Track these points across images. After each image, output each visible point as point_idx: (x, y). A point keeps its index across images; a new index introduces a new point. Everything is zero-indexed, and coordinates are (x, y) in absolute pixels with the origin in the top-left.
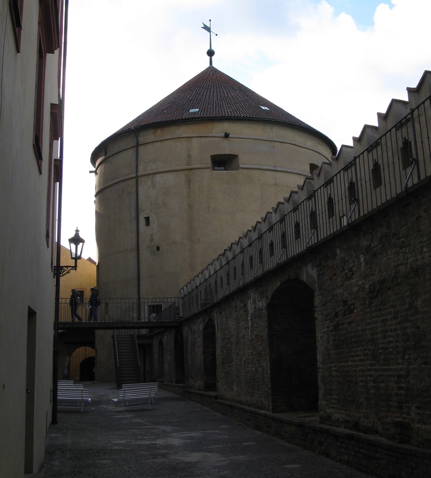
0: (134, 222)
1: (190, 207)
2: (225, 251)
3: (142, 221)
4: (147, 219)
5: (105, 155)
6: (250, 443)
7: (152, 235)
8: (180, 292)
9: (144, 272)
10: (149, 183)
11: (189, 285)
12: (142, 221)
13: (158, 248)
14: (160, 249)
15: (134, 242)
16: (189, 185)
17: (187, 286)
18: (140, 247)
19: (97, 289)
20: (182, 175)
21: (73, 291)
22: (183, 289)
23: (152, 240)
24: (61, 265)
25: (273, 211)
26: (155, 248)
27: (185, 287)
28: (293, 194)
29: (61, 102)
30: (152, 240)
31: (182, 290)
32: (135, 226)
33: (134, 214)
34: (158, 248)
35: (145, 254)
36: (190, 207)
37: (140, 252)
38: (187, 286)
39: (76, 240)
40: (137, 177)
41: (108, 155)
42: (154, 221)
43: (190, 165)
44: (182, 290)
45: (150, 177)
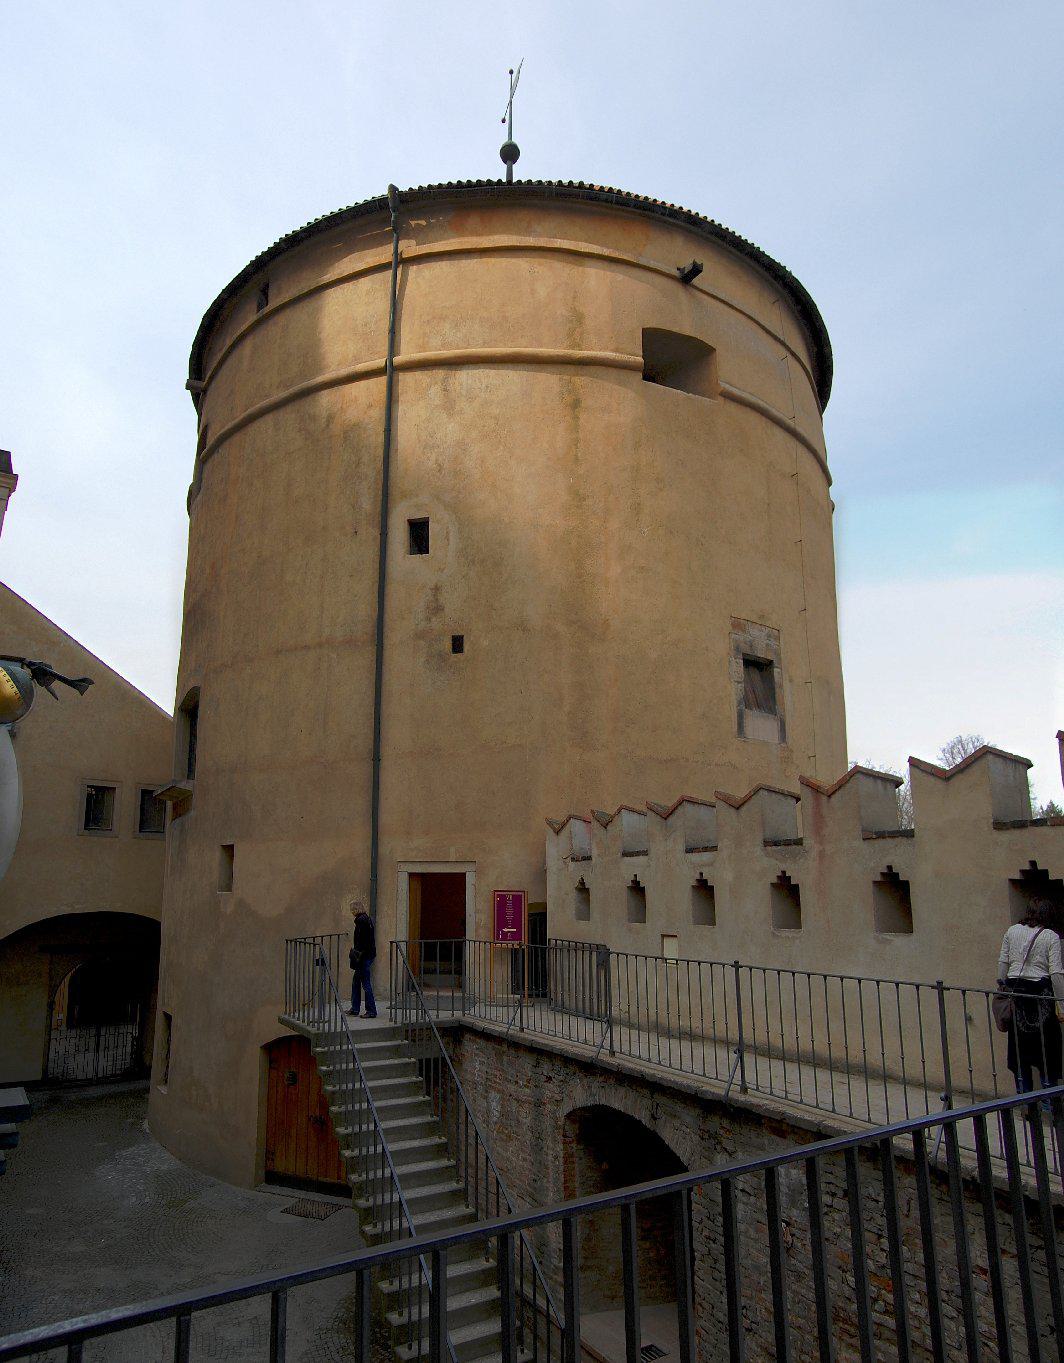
0: (371, 533)
3: (399, 535)
5: (260, 307)
6: (399, 1042)
7: (437, 589)
9: (397, 736)
10: (435, 391)
13: (458, 644)
14: (466, 647)
15: (365, 609)
16: (576, 418)
19: (946, 1170)
20: (548, 381)
21: (907, 883)
23: (436, 609)
26: (448, 645)
29: (198, 702)
30: (436, 609)
32: (371, 553)
34: (458, 644)
35: (403, 662)
36: (578, 498)
40: (391, 371)
41: (273, 304)
45: (440, 373)
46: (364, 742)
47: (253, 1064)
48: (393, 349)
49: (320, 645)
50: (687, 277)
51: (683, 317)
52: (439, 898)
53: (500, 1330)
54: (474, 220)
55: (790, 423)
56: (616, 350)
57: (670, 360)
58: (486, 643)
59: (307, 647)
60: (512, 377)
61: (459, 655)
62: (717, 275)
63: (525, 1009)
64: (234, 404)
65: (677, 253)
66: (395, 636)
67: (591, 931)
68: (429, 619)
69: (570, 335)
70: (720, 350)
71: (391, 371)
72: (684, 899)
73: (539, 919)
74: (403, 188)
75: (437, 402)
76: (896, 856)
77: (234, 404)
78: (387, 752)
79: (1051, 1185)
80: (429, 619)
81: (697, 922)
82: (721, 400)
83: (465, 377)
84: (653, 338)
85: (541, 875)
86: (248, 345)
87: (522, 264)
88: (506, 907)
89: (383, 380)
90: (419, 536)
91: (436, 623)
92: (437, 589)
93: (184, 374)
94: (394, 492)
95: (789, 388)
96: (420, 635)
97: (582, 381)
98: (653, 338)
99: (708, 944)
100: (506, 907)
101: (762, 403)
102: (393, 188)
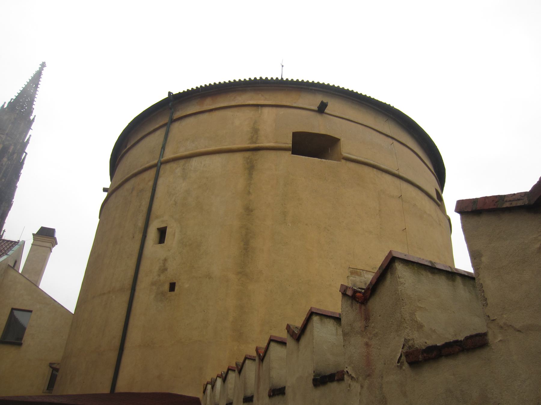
1: (249, 210)
2: (246, 358)
3: (152, 234)
4: (162, 233)
7: (165, 260)
8: (205, 391)
9: (135, 336)
11: (232, 376)
12: (152, 234)
13: (172, 287)
14: (176, 288)
17: (224, 380)
18: (138, 282)
20: (239, 158)
22: (213, 387)
23: (164, 270)
24: (7, 236)
25: (237, 367)
26: (167, 287)
27: (219, 382)
28: (272, 344)
30: (164, 270)
31: (209, 387)
33: (141, 223)
34: (172, 287)
35: (144, 296)
36: (249, 210)
37: (136, 294)
38: (224, 380)
39: (46, 236)
42: (174, 235)
43: (255, 143)
44: (209, 387)
45: (182, 162)
46: (117, 342)
49: (109, 292)
50: (322, 109)
53: (40, 287)
55: (397, 172)
56: (276, 142)
58: (187, 286)
59: (104, 294)
60: (218, 159)
61: (172, 293)
66: (142, 285)
68: (159, 275)
69: (252, 137)
70: (342, 140)
74: (175, 92)
75: (179, 174)
78: (128, 345)
80: (159, 275)
82: (343, 161)
83: (195, 162)
91: (162, 277)
92: (165, 260)
94: (153, 216)
95: (428, 181)
96: (153, 284)
98: (297, 136)
101: (372, 162)
102: (170, 93)
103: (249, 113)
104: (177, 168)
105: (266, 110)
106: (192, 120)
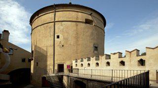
3: (56, 37)
10: (60, 24)
13: (63, 46)
34: (63, 46)
36: (77, 33)
40: (54, 22)
47: (41, 79)
48: (55, 20)
51: (90, 18)
52: (61, 67)
54: (65, 8)
57: (88, 22)
62: (94, 14)
63: (111, 76)
64: (34, 26)
65: (90, 12)
67: (77, 68)
71: (54, 22)
72: (87, 65)
73: (72, 67)
74: (72, 3)
76: (143, 58)
77: (34, 26)
79: (150, 82)
81: (107, 66)
84: (86, 20)
85: (72, 64)
86: (36, 20)
87: (71, 12)
88: (68, 66)
89: (53, 23)
90: (58, 37)
93: (29, 23)
97: (78, 23)
98: (86, 20)
99: (89, 68)
100: (68, 66)
103: (76, 13)
104: (60, 23)
105: (79, 13)
106: (61, 12)
